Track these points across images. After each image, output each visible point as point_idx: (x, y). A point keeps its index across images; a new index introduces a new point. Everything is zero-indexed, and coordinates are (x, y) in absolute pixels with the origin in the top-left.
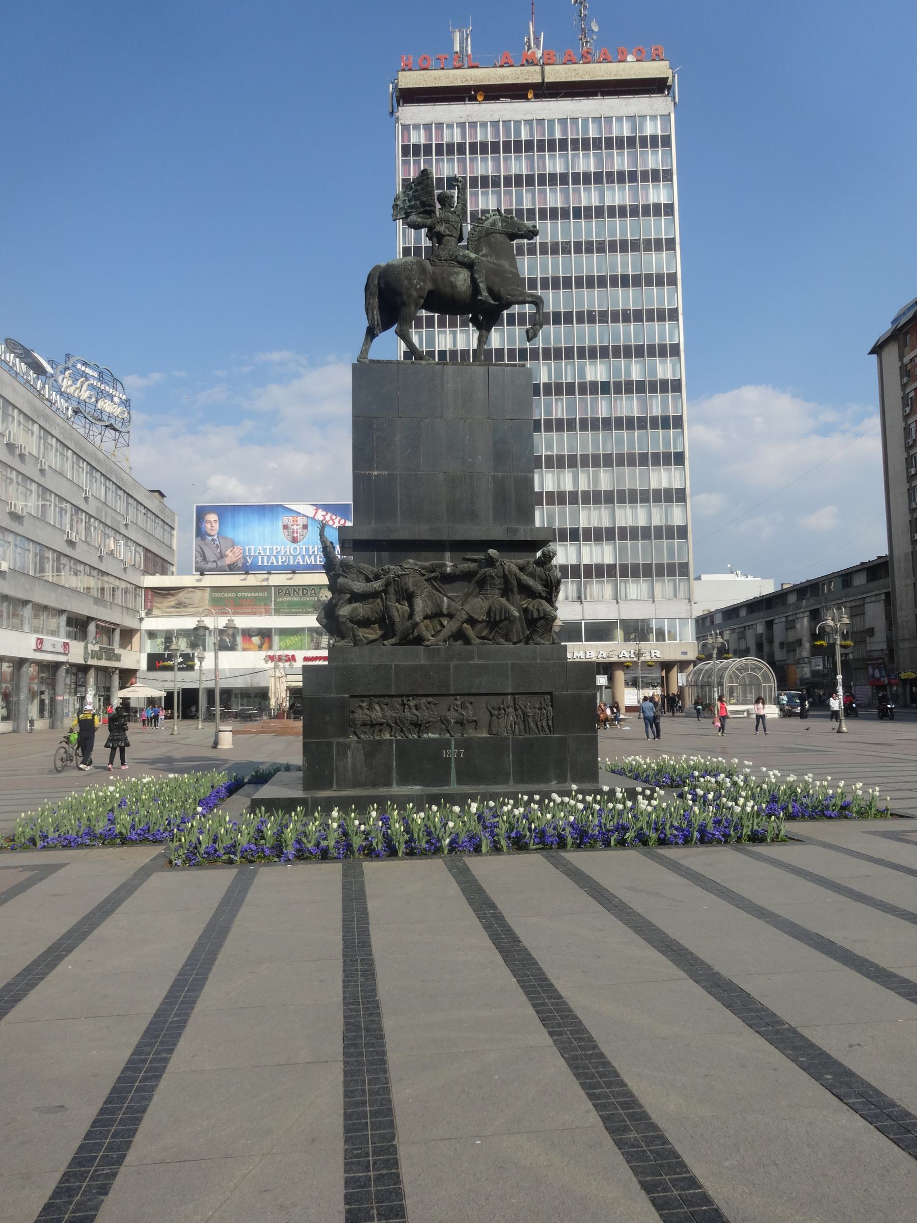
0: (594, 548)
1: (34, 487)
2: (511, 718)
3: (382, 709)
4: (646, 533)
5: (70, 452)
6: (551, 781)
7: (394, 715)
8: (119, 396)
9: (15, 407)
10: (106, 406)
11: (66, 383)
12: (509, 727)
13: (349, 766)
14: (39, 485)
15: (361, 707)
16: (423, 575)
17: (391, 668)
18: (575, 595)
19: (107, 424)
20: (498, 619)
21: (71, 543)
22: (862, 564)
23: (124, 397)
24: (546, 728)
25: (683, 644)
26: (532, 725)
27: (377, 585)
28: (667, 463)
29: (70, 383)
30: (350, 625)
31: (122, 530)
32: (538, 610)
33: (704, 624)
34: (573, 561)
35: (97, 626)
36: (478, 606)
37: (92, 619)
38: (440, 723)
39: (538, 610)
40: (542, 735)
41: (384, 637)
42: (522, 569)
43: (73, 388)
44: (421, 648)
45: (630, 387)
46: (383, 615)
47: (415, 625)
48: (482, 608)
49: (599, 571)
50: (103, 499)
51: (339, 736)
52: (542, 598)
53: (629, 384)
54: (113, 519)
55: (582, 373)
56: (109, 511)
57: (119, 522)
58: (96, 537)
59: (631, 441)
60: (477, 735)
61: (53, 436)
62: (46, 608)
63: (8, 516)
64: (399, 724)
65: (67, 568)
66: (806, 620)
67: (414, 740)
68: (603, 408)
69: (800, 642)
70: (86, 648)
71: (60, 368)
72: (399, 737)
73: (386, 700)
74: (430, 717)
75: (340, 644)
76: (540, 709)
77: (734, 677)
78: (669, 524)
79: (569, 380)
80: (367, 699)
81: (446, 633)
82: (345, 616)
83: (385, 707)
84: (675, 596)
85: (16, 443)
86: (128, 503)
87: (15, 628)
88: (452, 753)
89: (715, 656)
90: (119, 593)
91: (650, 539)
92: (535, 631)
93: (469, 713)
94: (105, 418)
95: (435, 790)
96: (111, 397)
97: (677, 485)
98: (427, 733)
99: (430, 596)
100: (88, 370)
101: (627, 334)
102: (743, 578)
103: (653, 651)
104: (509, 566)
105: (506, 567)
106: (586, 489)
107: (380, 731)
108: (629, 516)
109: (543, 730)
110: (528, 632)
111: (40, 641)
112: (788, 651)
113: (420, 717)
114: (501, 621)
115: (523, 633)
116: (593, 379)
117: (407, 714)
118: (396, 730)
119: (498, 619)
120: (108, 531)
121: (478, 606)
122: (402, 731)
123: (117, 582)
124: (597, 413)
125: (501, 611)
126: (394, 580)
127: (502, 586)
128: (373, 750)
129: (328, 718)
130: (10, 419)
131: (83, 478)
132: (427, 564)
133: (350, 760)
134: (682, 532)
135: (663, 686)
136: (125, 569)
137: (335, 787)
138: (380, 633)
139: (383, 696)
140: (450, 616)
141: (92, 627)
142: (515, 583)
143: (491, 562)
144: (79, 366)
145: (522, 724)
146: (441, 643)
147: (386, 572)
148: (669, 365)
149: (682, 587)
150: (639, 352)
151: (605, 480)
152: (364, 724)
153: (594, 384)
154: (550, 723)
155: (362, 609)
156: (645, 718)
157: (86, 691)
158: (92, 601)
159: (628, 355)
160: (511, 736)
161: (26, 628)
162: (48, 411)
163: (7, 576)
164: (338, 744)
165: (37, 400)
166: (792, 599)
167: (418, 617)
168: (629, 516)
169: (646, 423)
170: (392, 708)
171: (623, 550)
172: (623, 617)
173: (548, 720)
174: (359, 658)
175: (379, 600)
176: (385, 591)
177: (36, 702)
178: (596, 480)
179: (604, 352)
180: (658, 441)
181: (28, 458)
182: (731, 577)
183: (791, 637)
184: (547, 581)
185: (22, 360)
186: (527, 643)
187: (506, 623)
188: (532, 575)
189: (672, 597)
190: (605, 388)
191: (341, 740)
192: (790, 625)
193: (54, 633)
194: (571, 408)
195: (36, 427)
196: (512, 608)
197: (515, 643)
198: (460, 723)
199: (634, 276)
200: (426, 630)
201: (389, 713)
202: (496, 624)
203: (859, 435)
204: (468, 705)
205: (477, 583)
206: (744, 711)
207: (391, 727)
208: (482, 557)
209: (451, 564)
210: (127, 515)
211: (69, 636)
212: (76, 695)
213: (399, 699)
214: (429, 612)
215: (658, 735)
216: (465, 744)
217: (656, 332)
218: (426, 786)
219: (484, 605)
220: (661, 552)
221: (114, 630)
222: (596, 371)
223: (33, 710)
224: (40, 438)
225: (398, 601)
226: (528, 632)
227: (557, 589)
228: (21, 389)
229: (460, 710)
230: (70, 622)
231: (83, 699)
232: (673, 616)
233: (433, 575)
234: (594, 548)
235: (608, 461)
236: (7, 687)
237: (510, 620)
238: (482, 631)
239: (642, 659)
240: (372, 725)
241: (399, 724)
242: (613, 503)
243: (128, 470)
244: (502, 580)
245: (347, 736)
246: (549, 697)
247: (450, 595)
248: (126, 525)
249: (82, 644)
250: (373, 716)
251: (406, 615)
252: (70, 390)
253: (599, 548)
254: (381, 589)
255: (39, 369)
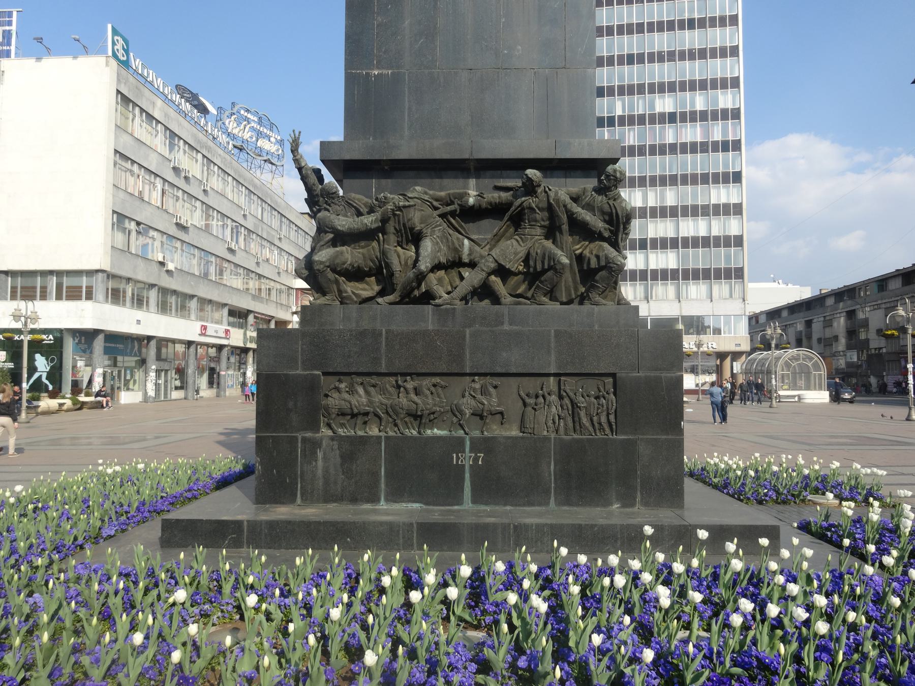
0: (659, 255)
1: (198, 204)
2: (554, 409)
3: (367, 393)
4: (706, 242)
5: (230, 178)
6: (612, 504)
7: (385, 401)
8: (274, 137)
9: (180, 138)
10: (263, 144)
11: (231, 125)
12: (550, 423)
13: (320, 472)
14: (203, 203)
15: (338, 389)
16: (436, 209)
17: (381, 334)
18: (642, 295)
19: (265, 158)
20: (539, 268)
21: (231, 250)
22: (897, 270)
23: (279, 138)
24: (606, 426)
25: (736, 337)
26: (585, 421)
27: (369, 221)
28: (726, 181)
29: (235, 125)
30: (331, 275)
31: (277, 242)
32: (598, 257)
33: (754, 320)
34: (641, 266)
35: (255, 317)
36: (512, 250)
37: (251, 311)
38: (450, 415)
39: (598, 257)
40: (600, 435)
41: (381, 294)
42: (575, 199)
43: (238, 129)
44: (429, 309)
45: (693, 117)
46: (380, 262)
47: (421, 277)
48: (516, 254)
49: (664, 275)
50: (260, 217)
51: (305, 429)
52: (601, 238)
53: (693, 113)
54: (268, 232)
55: (652, 105)
56: (265, 227)
57: (273, 236)
58: (254, 247)
59: (694, 163)
60: (507, 434)
61: (215, 164)
62: (210, 301)
63: (175, 226)
64: (392, 414)
65: (229, 270)
66: (842, 320)
67: (412, 438)
68: (670, 135)
69: (836, 338)
70: (245, 334)
71: (227, 113)
72: (391, 434)
73: (374, 380)
74: (435, 405)
75: (318, 302)
76: (597, 398)
77: (787, 365)
78: (727, 234)
79: (640, 112)
80: (348, 378)
81: (464, 288)
82: (321, 263)
83: (372, 389)
84: (731, 296)
85: (181, 167)
86: (281, 222)
87: (183, 317)
88: (467, 459)
89: (773, 346)
90: (273, 293)
91: (710, 247)
92: (593, 287)
93: (492, 402)
94: (265, 154)
95: (437, 513)
96: (269, 138)
97: (734, 200)
98: (432, 429)
99: (445, 238)
100: (249, 116)
101: (692, 70)
102: (783, 286)
103: (711, 343)
104: (556, 193)
105: (552, 194)
106: (654, 205)
107: (365, 423)
108: (690, 228)
109: (602, 429)
110: (583, 290)
111: (204, 328)
112: (825, 346)
113: (421, 406)
114: (544, 271)
115: (576, 289)
116: (662, 110)
117: (403, 400)
118: (388, 422)
119: (539, 268)
120: (265, 243)
121: (512, 250)
122: (396, 425)
123: (272, 284)
124: (665, 140)
125: (544, 258)
126: (394, 215)
127: (547, 223)
128: (352, 449)
129: (291, 404)
130: (176, 148)
131: (242, 200)
132: (443, 194)
133: (320, 463)
134: (738, 241)
135: (717, 373)
136: (279, 273)
137: (299, 501)
138: (377, 288)
139: (369, 374)
140: (472, 265)
141: (251, 318)
142: (564, 218)
143: (530, 188)
144: (242, 112)
145: (569, 420)
146: (458, 302)
147: (382, 203)
148: (730, 96)
149: (737, 288)
150: (703, 85)
151: (671, 197)
152: (342, 414)
153: (662, 115)
154: (612, 418)
155: (350, 255)
156: (712, 403)
157: (246, 368)
158: (250, 297)
159: (693, 88)
160: (553, 436)
161: (193, 317)
162: (210, 144)
163: (175, 275)
164: (304, 440)
165: (200, 134)
166: (830, 302)
167: (424, 265)
168: (690, 228)
169: (708, 147)
170: (383, 391)
171: (685, 258)
172: (684, 314)
173: (608, 414)
174: (341, 320)
175: (375, 244)
176: (382, 230)
177: (205, 376)
178: (663, 198)
179: (672, 87)
180: (719, 162)
181: (192, 181)
182: (775, 285)
183: (828, 333)
184: (611, 214)
185: (187, 101)
186: (581, 303)
187: (550, 274)
188: (589, 207)
189: (728, 296)
190: (672, 118)
191: (309, 435)
192: (828, 324)
193: (219, 322)
194: (642, 136)
195: (200, 156)
196: (559, 252)
197: (562, 303)
198: (479, 415)
199: (699, 19)
200: (437, 283)
201: (378, 398)
202: (537, 277)
203: (888, 171)
204: (492, 390)
205: (511, 219)
206: (794, 396)
207: (380, 418)
208: (520, 184)
209: (475, 193)
210: (281, 230)
211: (229, 324)
212: (239, 370)
213: (392, 379)
214: (443, 260)
215: (724, 418)
216: (484, 445)
217: (718, 68)
218: (426, 504)
219: (519, 249)
220: (720, 258)
221: (270, 321)
222: (665, 104)
223: (203, 381)
224: (203, 165)
225: (400, 244)
226: (583, 290)
227: (625, 228)
228: (185, 124)
229: (479, 396)
230: (232, 313)
231: (244, 374)
232: (722, 316)
233: (449, 208)
234: (659, 255)
235: (673, 180)
236: (180, 364)
237: (556, 270)
238: (517, 286)
239: (701, 349)
240: (354, 416)
241: (392, 414)
242: (677, 217)
243: (282, 196)
244: (546, 214)
245: (317, 429)
246: (611, 380)
247: (474, 237)
248: (280, 239)
249: (242, 331)
250: (354, 402)
251: (410, 262)
252: (235, 131)
253: (664, 255)
254: (374, 226)
255: (203, 110)
